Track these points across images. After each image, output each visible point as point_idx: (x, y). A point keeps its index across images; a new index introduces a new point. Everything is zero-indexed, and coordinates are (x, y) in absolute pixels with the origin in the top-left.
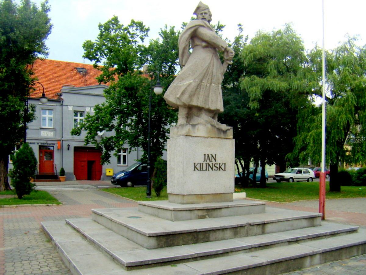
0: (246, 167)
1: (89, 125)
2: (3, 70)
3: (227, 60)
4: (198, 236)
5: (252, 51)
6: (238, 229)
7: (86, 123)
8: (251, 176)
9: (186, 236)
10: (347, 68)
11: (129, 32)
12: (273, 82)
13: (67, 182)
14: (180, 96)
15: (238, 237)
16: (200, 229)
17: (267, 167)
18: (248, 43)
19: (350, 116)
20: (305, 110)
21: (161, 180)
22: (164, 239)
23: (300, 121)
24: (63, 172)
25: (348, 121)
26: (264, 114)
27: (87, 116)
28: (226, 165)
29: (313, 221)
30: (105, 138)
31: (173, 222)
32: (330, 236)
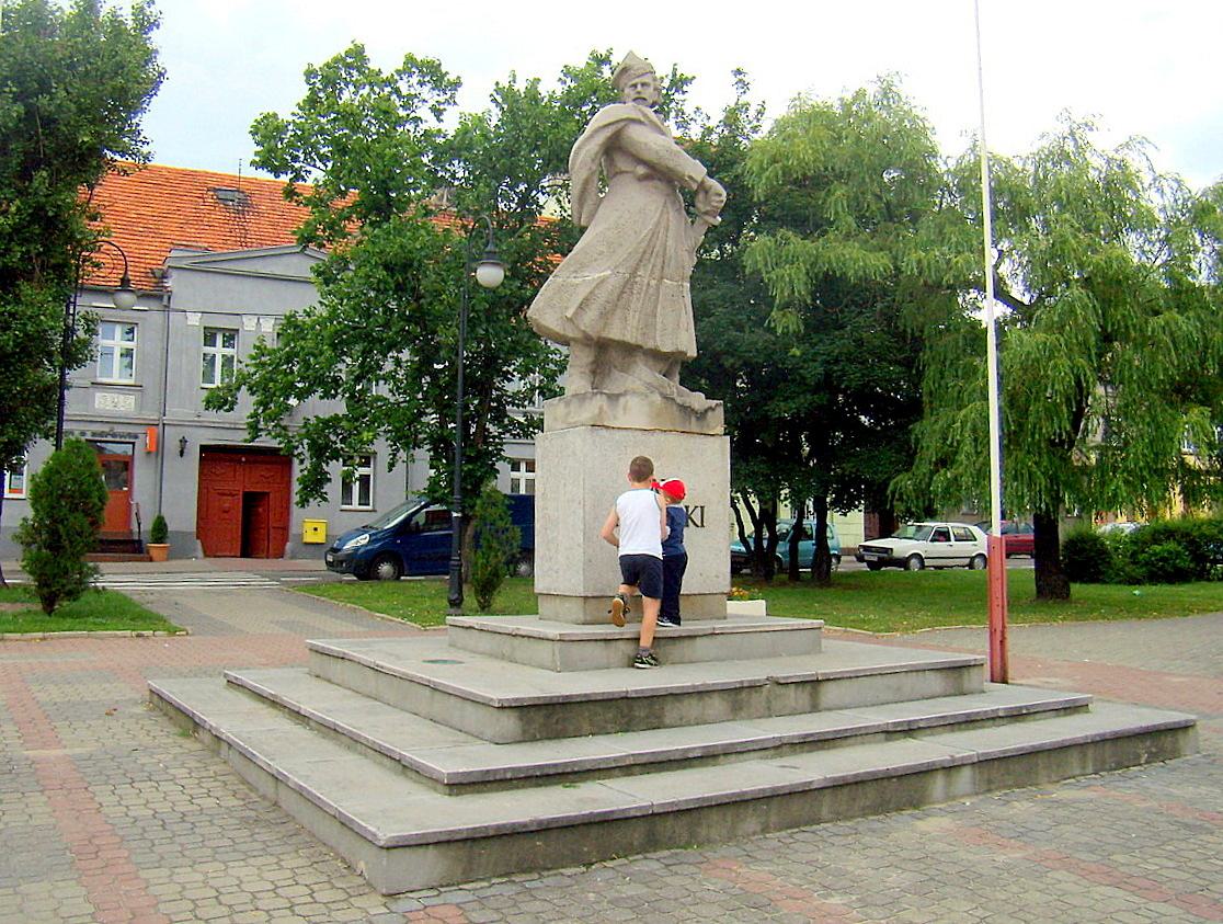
0: (767, 518)
1: (262, 377)
2: (8, 205)
3: (706, 213)
5: (778, 157)
6: (744, 695)
7: (252, 370)
8: (782, 549)
9: (599, 709)
10: (1067, 215)
11: (397, 91)
12: (845, 252)
13: (175, 564)
14: (575, 313)
15: (743, 718)
17: (834, 518)
18: (767, 125)
19: (1082, 361)
20: (947, 339)
21: (496, 556)
22: (539, 717)
23: (931, 372)
25: (1078, 383)
26: (821, 348)
27: (258, 348)
28: (705, 509)
29: (961, 676)
30: (313, 421)
32: (1005, 721)
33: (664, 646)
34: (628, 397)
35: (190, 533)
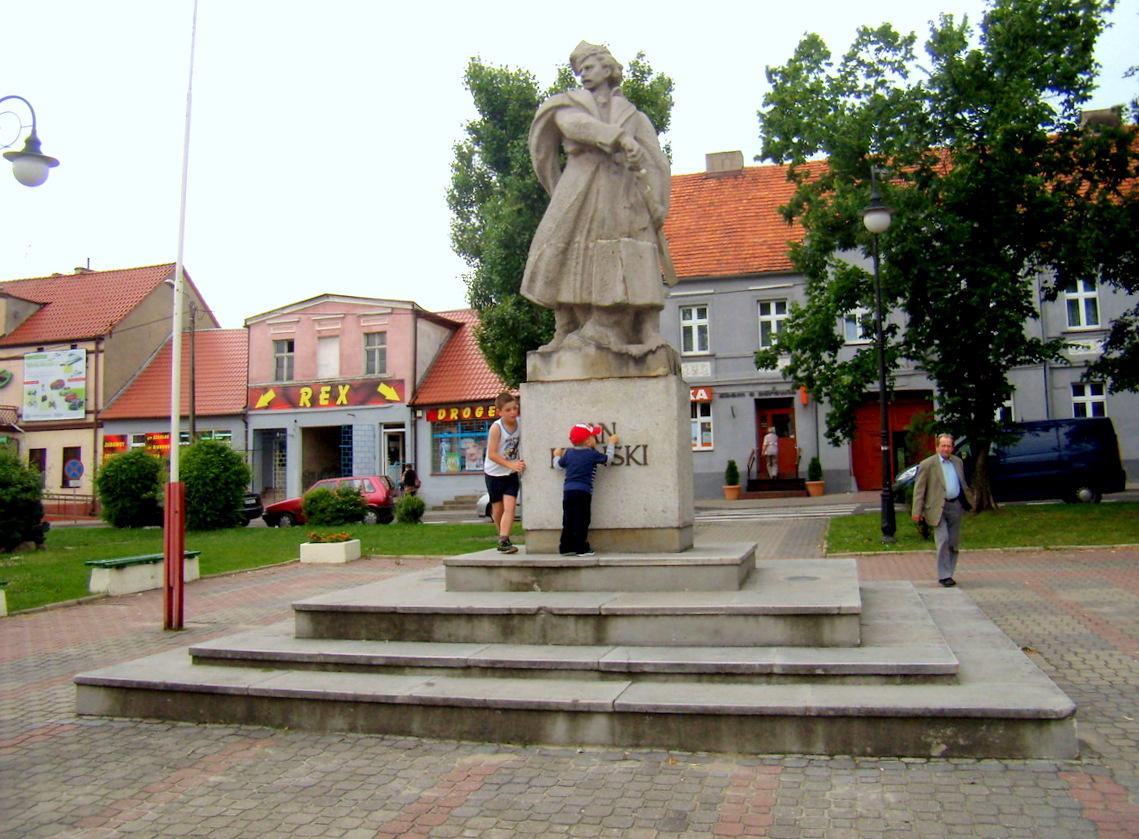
4: (402, 624)
6: (515, 621)
16: (404, 608)
22: (326, 621)
24: (816, 470)
28: (648, 449)
31: (542, 605)
33: (547, 574)
34: (561, 353)
35: (844, 471)
